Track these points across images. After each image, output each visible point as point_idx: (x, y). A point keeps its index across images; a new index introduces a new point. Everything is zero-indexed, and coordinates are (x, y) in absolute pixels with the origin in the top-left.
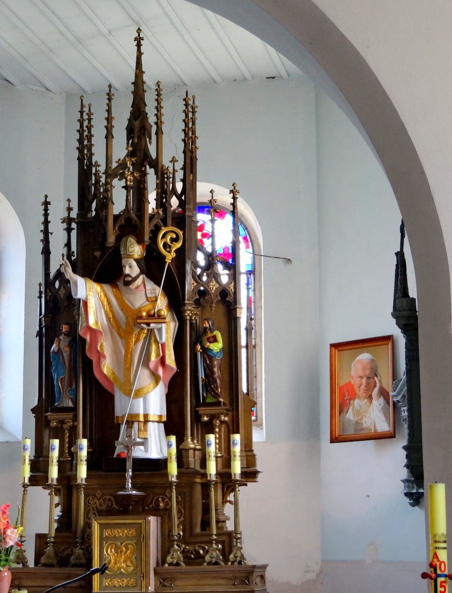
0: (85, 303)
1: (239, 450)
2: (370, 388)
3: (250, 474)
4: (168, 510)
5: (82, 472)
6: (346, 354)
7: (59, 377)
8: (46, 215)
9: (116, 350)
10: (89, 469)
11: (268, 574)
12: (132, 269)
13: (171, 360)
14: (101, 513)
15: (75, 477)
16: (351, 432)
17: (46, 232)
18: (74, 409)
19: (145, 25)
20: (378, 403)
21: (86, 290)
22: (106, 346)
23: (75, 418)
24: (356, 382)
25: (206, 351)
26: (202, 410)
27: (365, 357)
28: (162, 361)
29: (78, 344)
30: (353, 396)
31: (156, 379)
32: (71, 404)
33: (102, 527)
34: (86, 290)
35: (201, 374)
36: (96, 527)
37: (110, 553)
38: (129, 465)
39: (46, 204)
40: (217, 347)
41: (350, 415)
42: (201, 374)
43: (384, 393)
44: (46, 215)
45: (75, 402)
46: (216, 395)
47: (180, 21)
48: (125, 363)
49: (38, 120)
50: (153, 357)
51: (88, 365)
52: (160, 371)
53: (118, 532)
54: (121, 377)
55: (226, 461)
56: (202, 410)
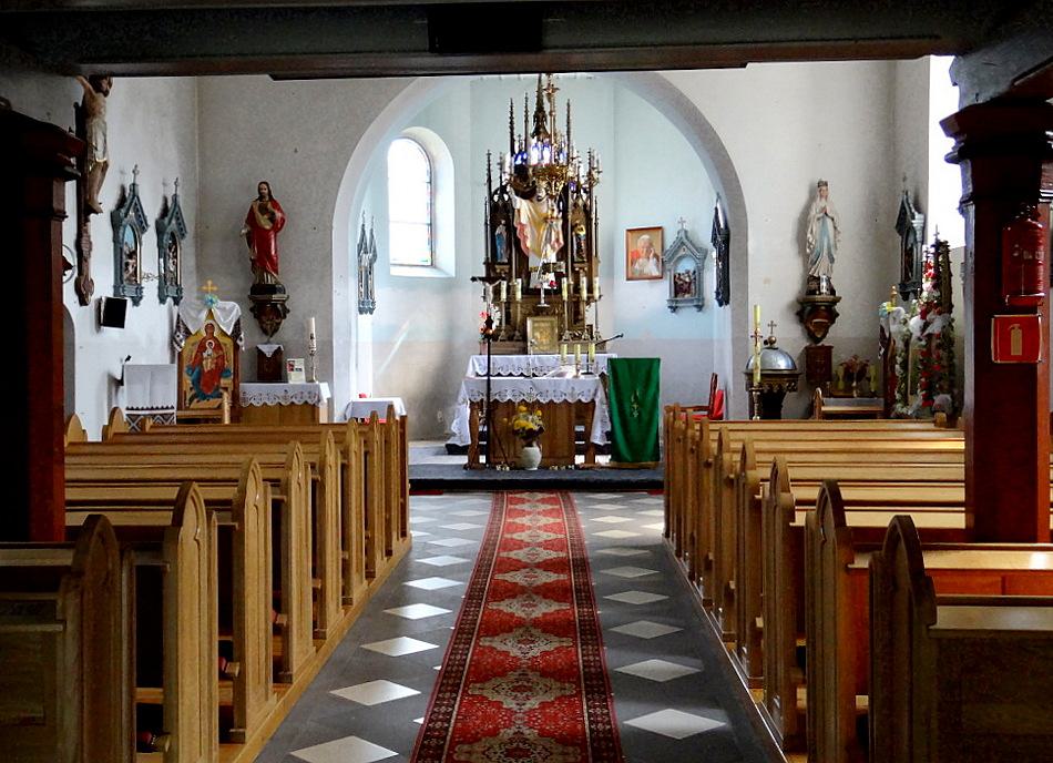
0: (519, 211)
1: (730, 338)
2: (648, 252)
3: (590, 299)
4: (560, 315)
5: (519, 295)
6: (635, 234)
7: (501, 249)
8: (489, 161)
9: (533, 233)
10: (523, 293)
11: (664, 374)
12: (543, 194)
13: (561, 241)
14: (530, 315)
15: (515, 298)
16: (637, 275)
17: (489, 170)
18: (510, 263)
19: (214, 56)
20: (653, 261)
21: (522, 205)
22: (528, 231)
23: (511, 269)
24: (640, 250)
25: (577, 235)
26: (575, 265)
27: (646, 237)
28: (557, 240)
29: (511, 229)
30: (639, 257)
31: (553, 248)
32: (506, 261)
33: (534, 322)
34: (522, 205)
35: (575, 247)
36: (529, 323)
37: (537, 334)
38: (542, 292)
39: (489, 154)
40: (583, 233)
41: (637, 266)
42: (575, 247)
43: (656, 256)
44: (489, 161)
45: (510, 259)
46: (582, 258)
47: (626, 46)
48: (537, 241)
49: (820, 145)
50: (553, 239)
51: (518, 242)
52: (556, 245)
53: (542, 325)
54: (537, 249)
55: (577, 289)
56: (575, 265)
